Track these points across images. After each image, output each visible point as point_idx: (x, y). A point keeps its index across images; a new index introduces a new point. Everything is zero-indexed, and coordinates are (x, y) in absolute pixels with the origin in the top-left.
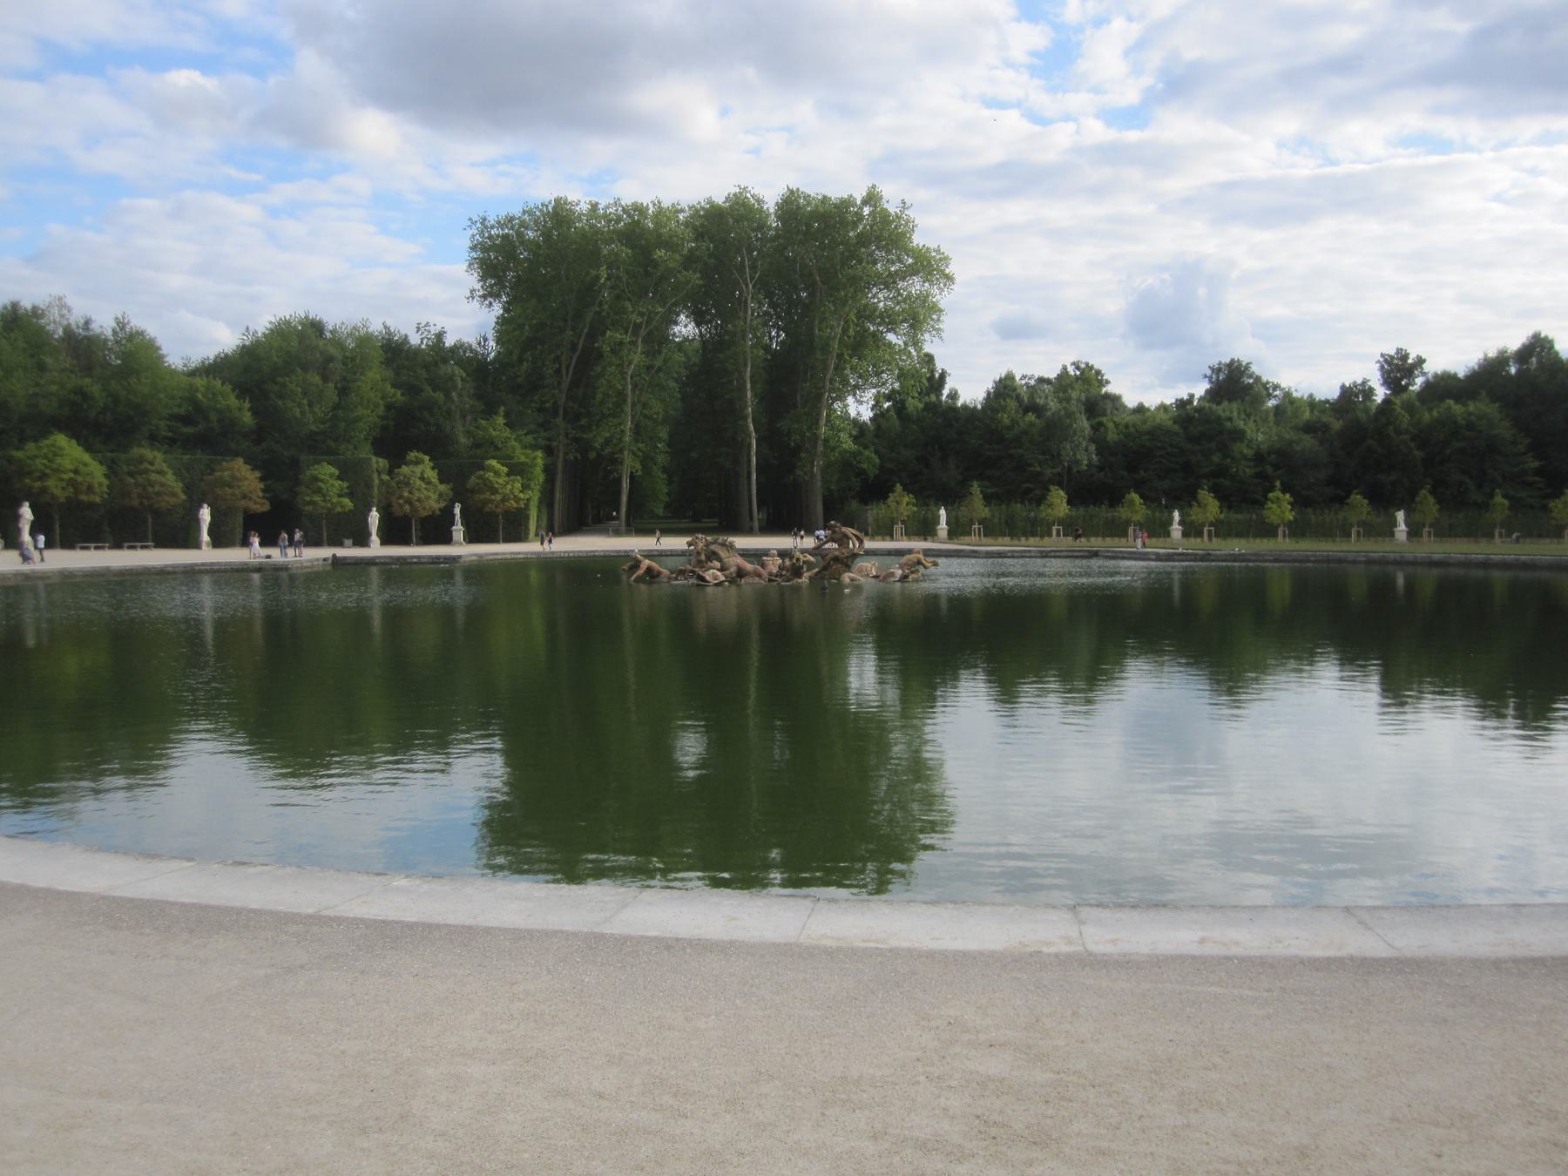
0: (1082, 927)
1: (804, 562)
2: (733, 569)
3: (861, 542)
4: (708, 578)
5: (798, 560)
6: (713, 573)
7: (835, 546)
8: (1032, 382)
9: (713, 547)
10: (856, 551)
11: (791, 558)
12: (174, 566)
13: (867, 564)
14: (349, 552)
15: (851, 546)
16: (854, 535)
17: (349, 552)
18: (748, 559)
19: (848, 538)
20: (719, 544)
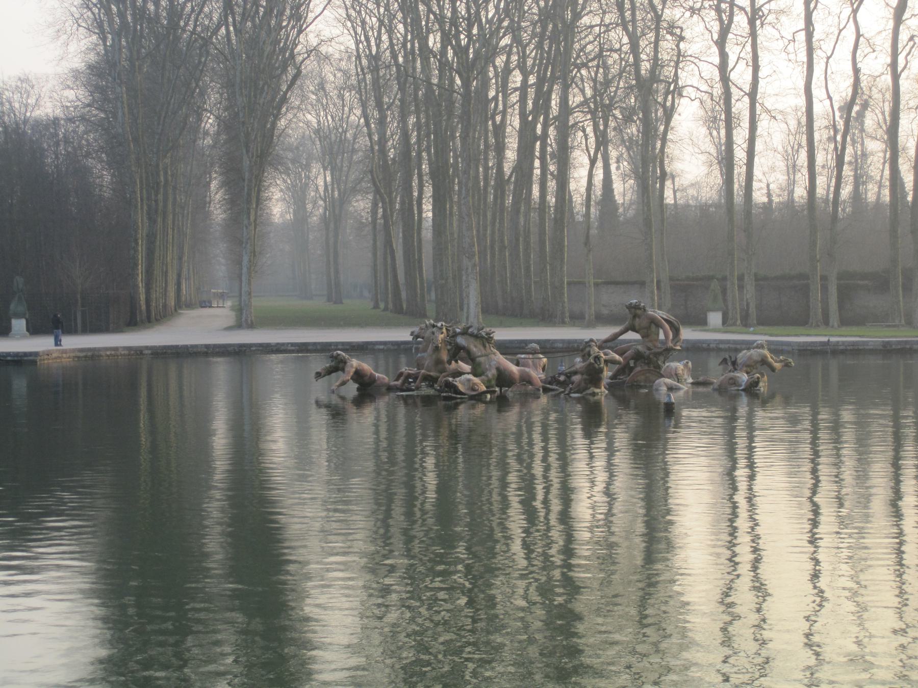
0: (905, 645)
1: (606, 362)
2: (492, 373)
3: (676, 332)
4: (461, 388)
5: (597, 358)
6: (469, 380)
7: (636, 336)
8: (223, 137)
9: (461, 340)
10: (670, 344)
11: (586, 355)
12: (165, 347)
13: (678, 364)
14: (79, 304)
15: (662, 336)
16: (666, 320)
17: (79, 304)
18: (509, 357)
19: (658, 325)
20: (472, 335)
